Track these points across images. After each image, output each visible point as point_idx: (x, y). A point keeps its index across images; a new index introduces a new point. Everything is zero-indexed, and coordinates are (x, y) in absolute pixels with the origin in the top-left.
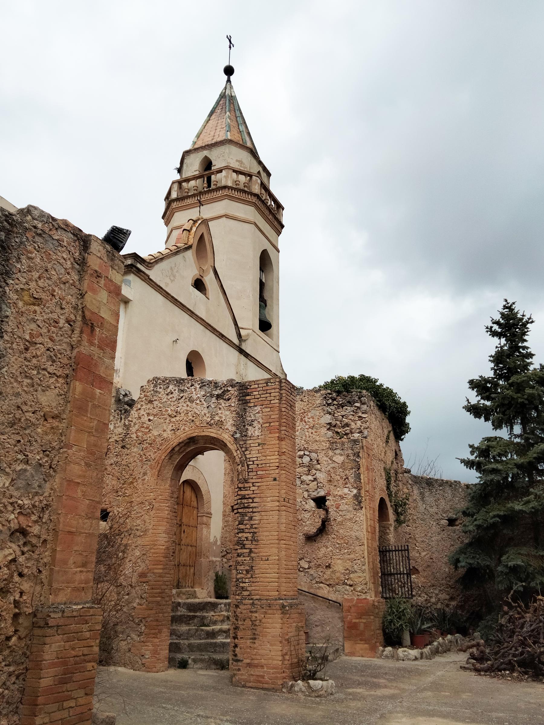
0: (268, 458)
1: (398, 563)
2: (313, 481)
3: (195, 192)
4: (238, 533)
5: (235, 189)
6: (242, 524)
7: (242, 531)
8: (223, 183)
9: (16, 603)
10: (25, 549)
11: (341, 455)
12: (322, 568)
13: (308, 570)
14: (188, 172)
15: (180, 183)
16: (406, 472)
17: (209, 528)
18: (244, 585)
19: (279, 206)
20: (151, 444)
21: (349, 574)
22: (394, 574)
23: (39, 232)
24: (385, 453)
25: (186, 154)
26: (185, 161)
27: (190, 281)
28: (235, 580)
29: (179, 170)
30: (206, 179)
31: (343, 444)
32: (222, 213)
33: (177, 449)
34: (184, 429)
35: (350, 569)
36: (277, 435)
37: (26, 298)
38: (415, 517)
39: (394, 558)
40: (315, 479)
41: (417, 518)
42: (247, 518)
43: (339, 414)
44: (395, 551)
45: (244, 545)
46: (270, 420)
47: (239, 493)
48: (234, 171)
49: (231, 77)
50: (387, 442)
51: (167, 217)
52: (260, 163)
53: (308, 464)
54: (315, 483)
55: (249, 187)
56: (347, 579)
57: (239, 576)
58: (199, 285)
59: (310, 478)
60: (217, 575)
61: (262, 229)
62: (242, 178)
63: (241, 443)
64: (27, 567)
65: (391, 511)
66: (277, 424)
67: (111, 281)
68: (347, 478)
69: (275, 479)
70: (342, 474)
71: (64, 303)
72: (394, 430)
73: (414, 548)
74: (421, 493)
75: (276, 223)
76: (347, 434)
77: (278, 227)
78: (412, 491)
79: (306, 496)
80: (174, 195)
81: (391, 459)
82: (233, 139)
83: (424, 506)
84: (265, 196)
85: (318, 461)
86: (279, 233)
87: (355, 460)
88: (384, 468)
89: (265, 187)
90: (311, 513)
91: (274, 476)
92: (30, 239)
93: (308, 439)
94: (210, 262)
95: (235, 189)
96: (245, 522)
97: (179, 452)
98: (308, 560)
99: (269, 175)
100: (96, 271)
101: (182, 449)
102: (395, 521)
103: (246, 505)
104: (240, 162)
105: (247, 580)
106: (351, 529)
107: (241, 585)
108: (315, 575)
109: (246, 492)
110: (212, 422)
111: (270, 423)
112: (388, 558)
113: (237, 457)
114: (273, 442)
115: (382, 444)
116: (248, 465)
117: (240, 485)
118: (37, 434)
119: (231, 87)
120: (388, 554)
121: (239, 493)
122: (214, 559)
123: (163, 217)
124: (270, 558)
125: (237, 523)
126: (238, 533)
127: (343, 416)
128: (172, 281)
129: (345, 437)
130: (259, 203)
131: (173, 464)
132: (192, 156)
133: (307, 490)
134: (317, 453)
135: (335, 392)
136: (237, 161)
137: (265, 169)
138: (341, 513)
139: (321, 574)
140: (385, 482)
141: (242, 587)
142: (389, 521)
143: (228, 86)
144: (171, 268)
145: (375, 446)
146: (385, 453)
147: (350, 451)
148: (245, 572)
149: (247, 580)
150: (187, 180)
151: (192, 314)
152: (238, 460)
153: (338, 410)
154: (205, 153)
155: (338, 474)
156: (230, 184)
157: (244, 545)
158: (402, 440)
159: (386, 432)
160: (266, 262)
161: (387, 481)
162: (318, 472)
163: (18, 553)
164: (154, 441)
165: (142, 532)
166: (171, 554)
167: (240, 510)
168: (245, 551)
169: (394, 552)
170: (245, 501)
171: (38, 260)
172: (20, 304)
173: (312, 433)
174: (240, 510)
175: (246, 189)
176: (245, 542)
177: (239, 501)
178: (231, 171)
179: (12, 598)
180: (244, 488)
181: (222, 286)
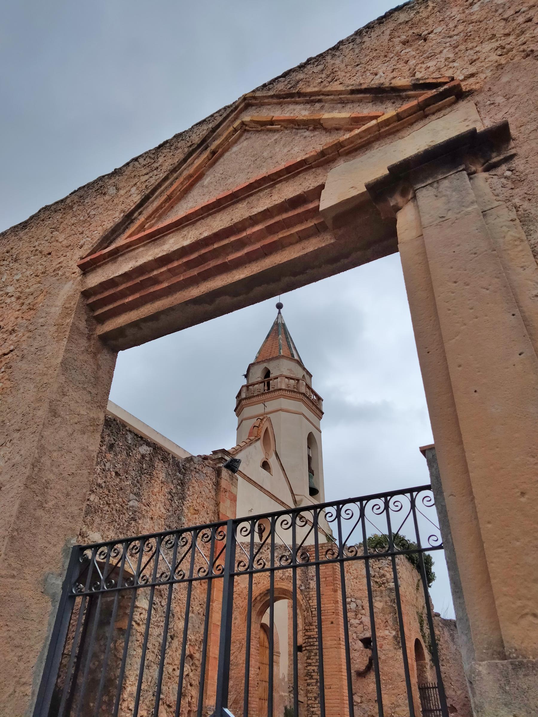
0: (326, 605)
1: (436, 700)
2: (360, 624)
3: (259, 393)
4: (307, 667)
5: (287, 390)
6: (310, 659)
7: (310, 664)
8: (279, 387)
9: (189, 703)
10: (193, 668)
11: (381, 601)
12: (372, 702)
13: (361, 704)
14: (253, 380)
15: (247, 386)
16: (436, 616)
17: (279, 666)
18: (313, 709)
19: (319, 399)
20: (240, 594)
21: (395, 708)
22: (434, 710)
23: (197, 470)
24: (417, 599)
25: (251, 366)
26: (251, 370)
27: (260, 463)
28: (306, 705)
29: (246, 376)
30: (266, 384)
31: (381, 592)
32: (279, 408)
33: (258, 598)
34: (263, 583)
35: (395, 703)
36: (332, 587)
37: (192, 511)
38: (448, 658)
39: (433, 695)
40: (361, 623)
41: (450, 658)
42: (313, 654)
43: (377, 566)
44: (433, 688)
45: (312, 676)
46: (326, 576)
47: (306, 633)
48: (286, 378)
49: (281, 310)
50: (417, 589)
51: (238, 410)
52: (304, 369)
53: (355, 610)
54: (362, 626)
55: (297, 389)
56: (394, 713)
57: (310, 702)
58: (265, 465)
59: (358, 621)
60: (286, 708)
61: (308, 417)
62: (292, 382)
63: (306, 594)
64: (194, 680)
65: (426, 652)
66: (332, 578)
67: (232, 493)
68: (387, 621)
69: (332, 623)
70: (383, 618)
71: (208, 510)
72: (423, 578)
73: (450, 687)
74: (451, 635)
75: (318, 412)
76: (384, 583)
77: (320, 413)
78: (443, 633)
79: (355, 637)
80: (243, 395)
81: (422, 604)
82: (285, 355)
83: (455, 646)
84: (309, 393)
85: (362, 606)
86: (320, 418)
87: (392, 606)
88: (417, 613)
89: (309, 387)
90: (360, 652)
91: (331, 620)
92: (193, 475)
93: (353, 587)
94: (272, 447)
95: (287, 390)
96: (312, 657)
97: (260, 601)
98: (360, 695)
99: (311, 376)
100: (224, 489)
101: (262, 599)
102: (430, 660)
103: (312, 643)
104: (290, 370)
105: (315, 706)
106: (393, 666)
107: (312, 709)
108: (367, 709)
109: (311, 633)
110: (284, 577)
111: (326, 578)
112: (427, 695)
113: (303, 605)
114: (329, 593)
115: (414, 591)
116: (312, 612)
117: (307, 628)
118: (197, 593)
119: (282, 317)
120: (427, 692)
121: (306, 633)
122: (283, 694)
123: (235, 411)
124: (332, 687)
125: (306, 658)
126: (307, 667)
127: (380, 568)
128: (247, 465)
129: (383, 586)
130: (305, 399)
131: (256, 610)
132: (256, 367)
133: (355, 632)
134: (361, 600)
135: (372, 548)
136: (288, 369)
137: (308, 372)
138: (384, 652)
139: (371, 708)
140: (419, 625)
141: (313, 712)
142: (425, 659)
143: (280, 317)
144: (247, 456)
145: (408, 593)
146: (417, 599)
147: (388, 598)
148: (313, 699)
149: (315, 706)
150: (253, 385)
151: (261, 488)
152: (304, 607)
153: (376, 563)
154: (265, 365)
155: (379, 618)
156: (283, 387)
157: (312, 676)
158: (430, 587)
159: (416, 581)
160: (312, 441)
161: (421, 624)
162: (363, 616)
163: (190, 671)
164: (242, 592)
165: (235, 665)
166: (256, 684)
167: (307, 648)
168: (313, 681)
169: (431, 686)
170: (311, 640)
171: (197, 487)
172: (189, 515)
173: (356, 583)
174: (307, 648)
175: (295, 390)
176: (312, 674)
177: (306, 640)
178: (284, 378)
179: (187, 700)
180: (310, 629)
181: (281, 464)
